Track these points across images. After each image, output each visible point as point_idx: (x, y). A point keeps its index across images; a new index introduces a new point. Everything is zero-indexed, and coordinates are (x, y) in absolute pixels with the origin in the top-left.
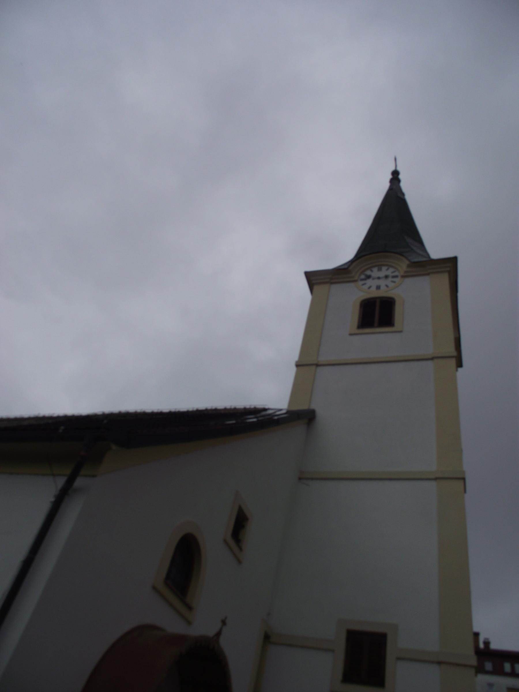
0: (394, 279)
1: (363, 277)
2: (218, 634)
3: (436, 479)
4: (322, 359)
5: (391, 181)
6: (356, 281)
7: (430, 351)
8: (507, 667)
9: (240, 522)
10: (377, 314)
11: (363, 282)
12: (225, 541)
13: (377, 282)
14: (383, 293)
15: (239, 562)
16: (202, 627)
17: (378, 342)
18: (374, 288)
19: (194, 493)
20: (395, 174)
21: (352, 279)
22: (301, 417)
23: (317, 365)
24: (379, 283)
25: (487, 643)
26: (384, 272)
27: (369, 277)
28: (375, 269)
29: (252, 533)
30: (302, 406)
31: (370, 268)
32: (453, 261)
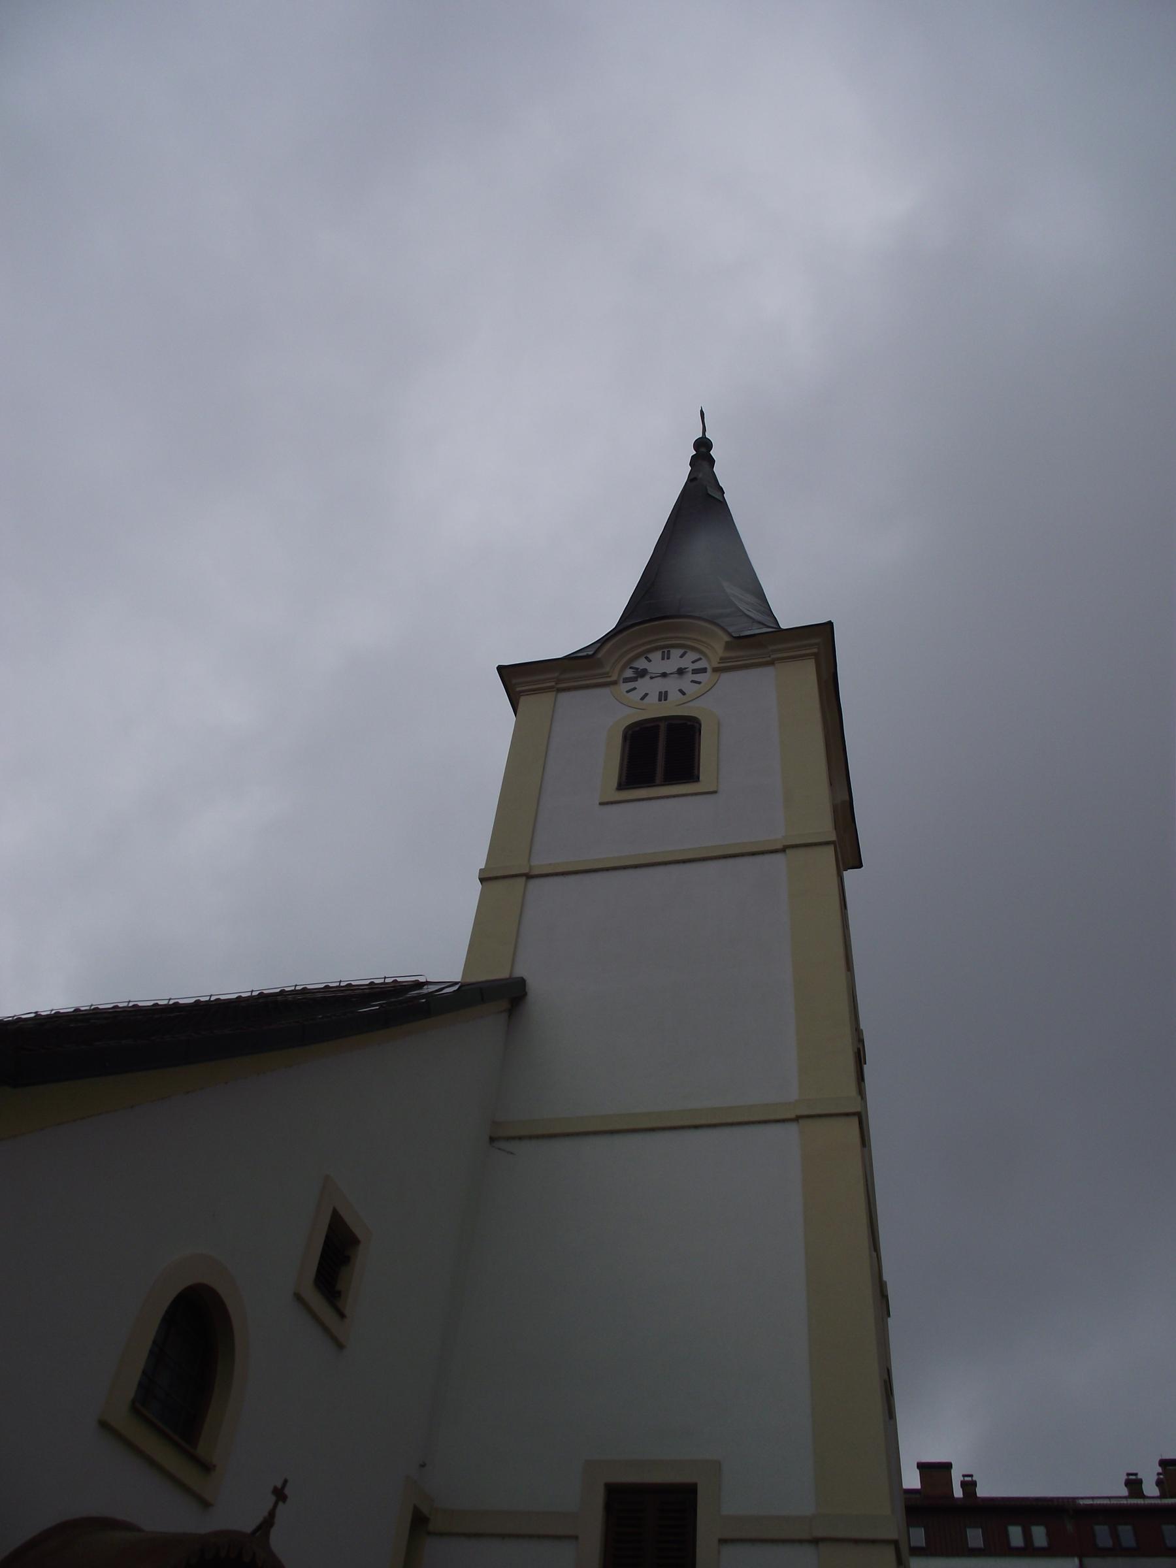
0: (697, 677)
1: (629, 673)
2: (268, 1523)
3: (797, 1119)
4: (540, 862)
5: (694, 461)
6: (615, 683)
7: (778, 834)
8: (1015, 1535)
9: (337, 1252)
10: (661, 755)
11: (631, 685)
12: (298, 1297)
13: (660, 685)
14: (670, 709)
15: (340, 1346)
16: (235, 1510)
17: (666, 817)
18: (653, 698)
19: (222, 1195)
20: (703, 447)
21: (609, 680)
22: (494, 997)
23: (529, 876)
24: (663, 688)
25: (969, 1485)
26: (676, 661)
27: (642, 673)
28: (656, 656)
29: (368, 1275)
30: (500, 973)
31: (645, 654)
32: (825, 631)
